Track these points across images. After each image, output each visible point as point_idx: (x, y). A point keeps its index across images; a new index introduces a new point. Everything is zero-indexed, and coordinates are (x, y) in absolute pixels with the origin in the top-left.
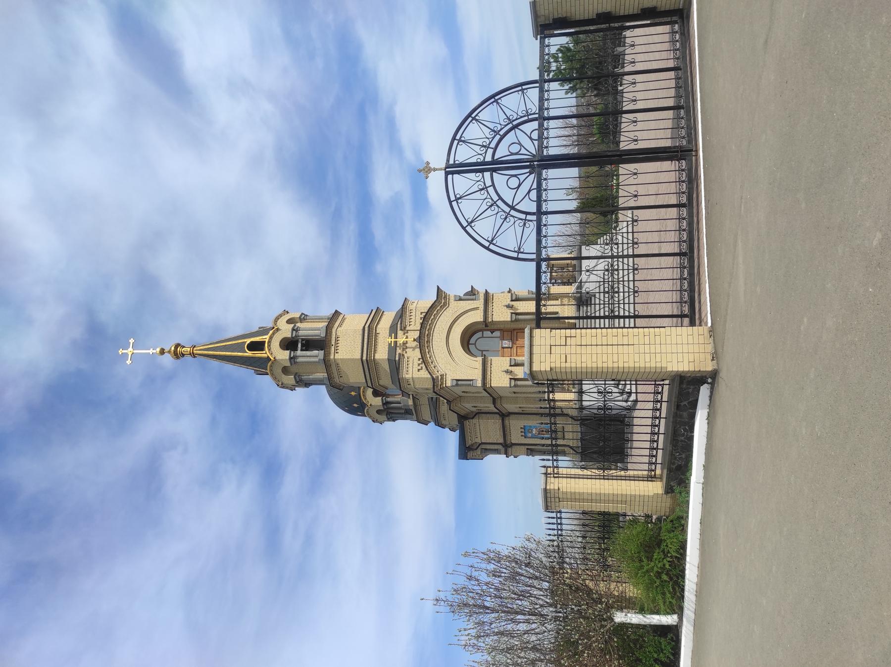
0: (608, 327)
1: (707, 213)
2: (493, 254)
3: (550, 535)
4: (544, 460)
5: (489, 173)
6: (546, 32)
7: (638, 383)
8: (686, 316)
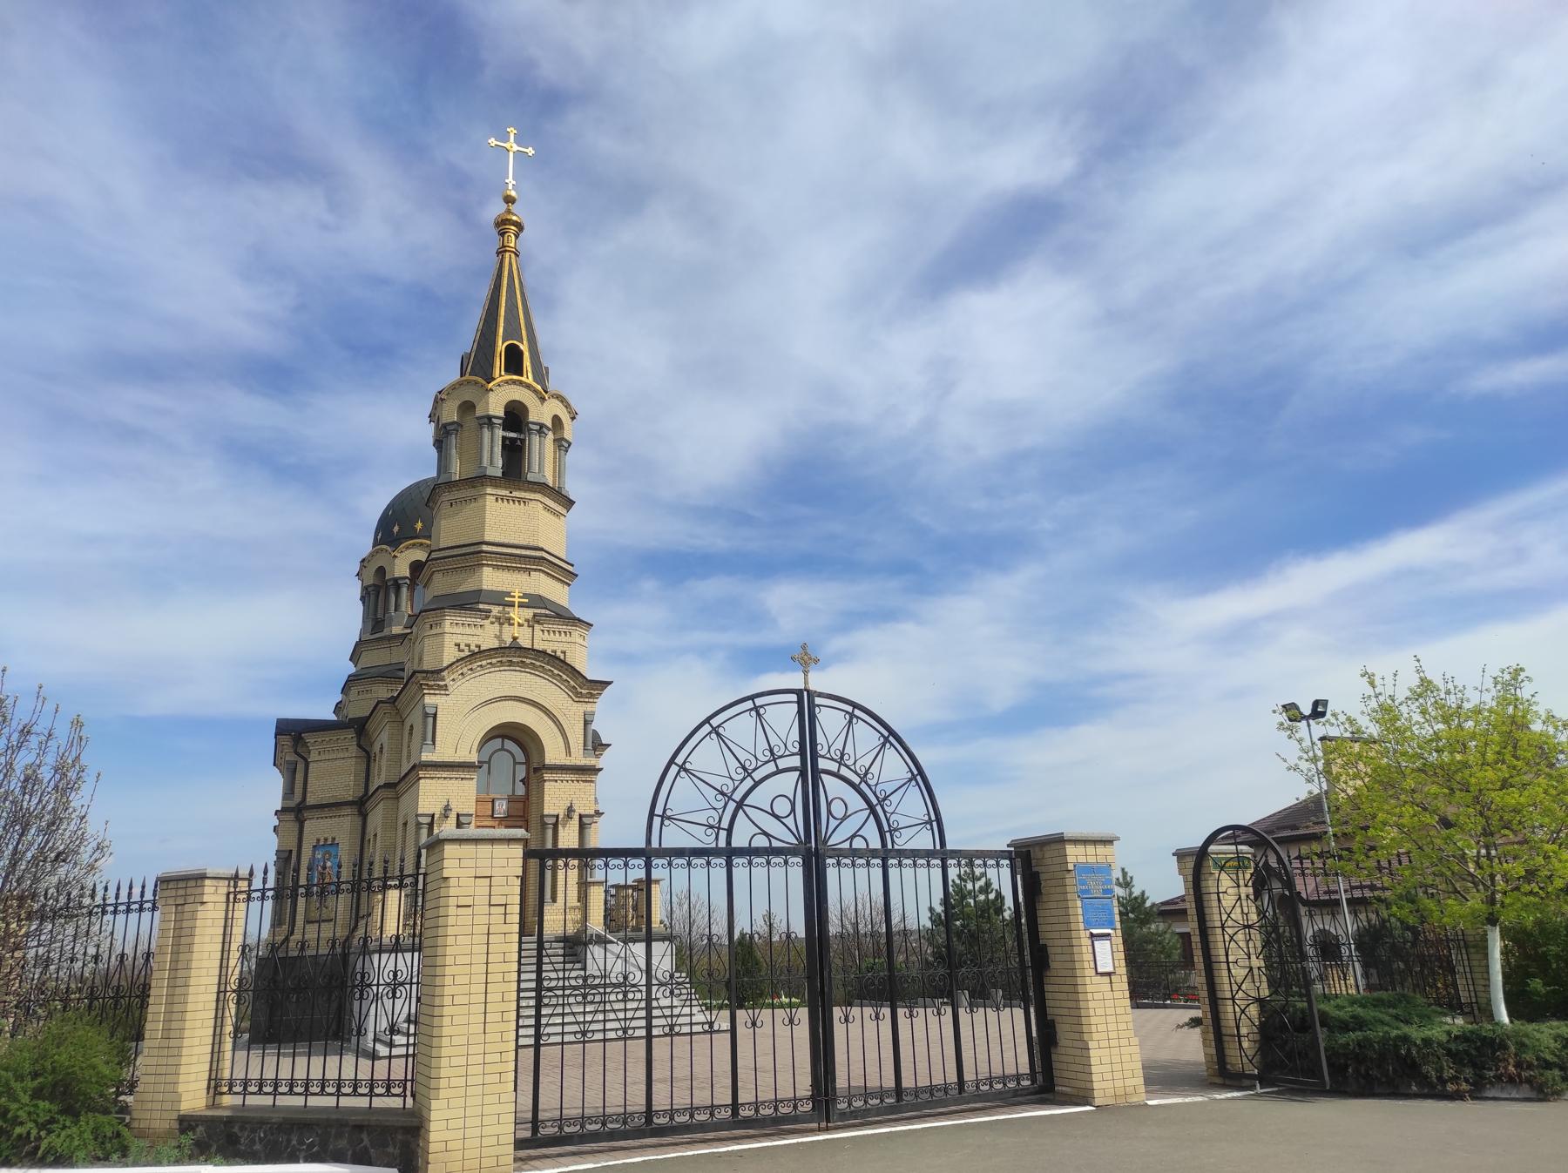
0: (522, 962)
1: (720, 1155)
2: (664, 767)
3: (106, 889)
4: (266, 872)
5: (799, 765)
6: (1018, 862)
7: (410, 1060)
8: (535, 1130)
